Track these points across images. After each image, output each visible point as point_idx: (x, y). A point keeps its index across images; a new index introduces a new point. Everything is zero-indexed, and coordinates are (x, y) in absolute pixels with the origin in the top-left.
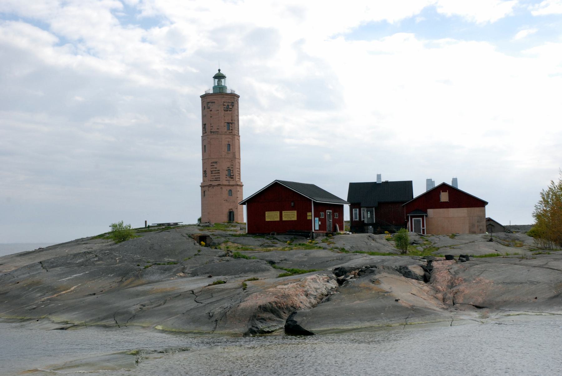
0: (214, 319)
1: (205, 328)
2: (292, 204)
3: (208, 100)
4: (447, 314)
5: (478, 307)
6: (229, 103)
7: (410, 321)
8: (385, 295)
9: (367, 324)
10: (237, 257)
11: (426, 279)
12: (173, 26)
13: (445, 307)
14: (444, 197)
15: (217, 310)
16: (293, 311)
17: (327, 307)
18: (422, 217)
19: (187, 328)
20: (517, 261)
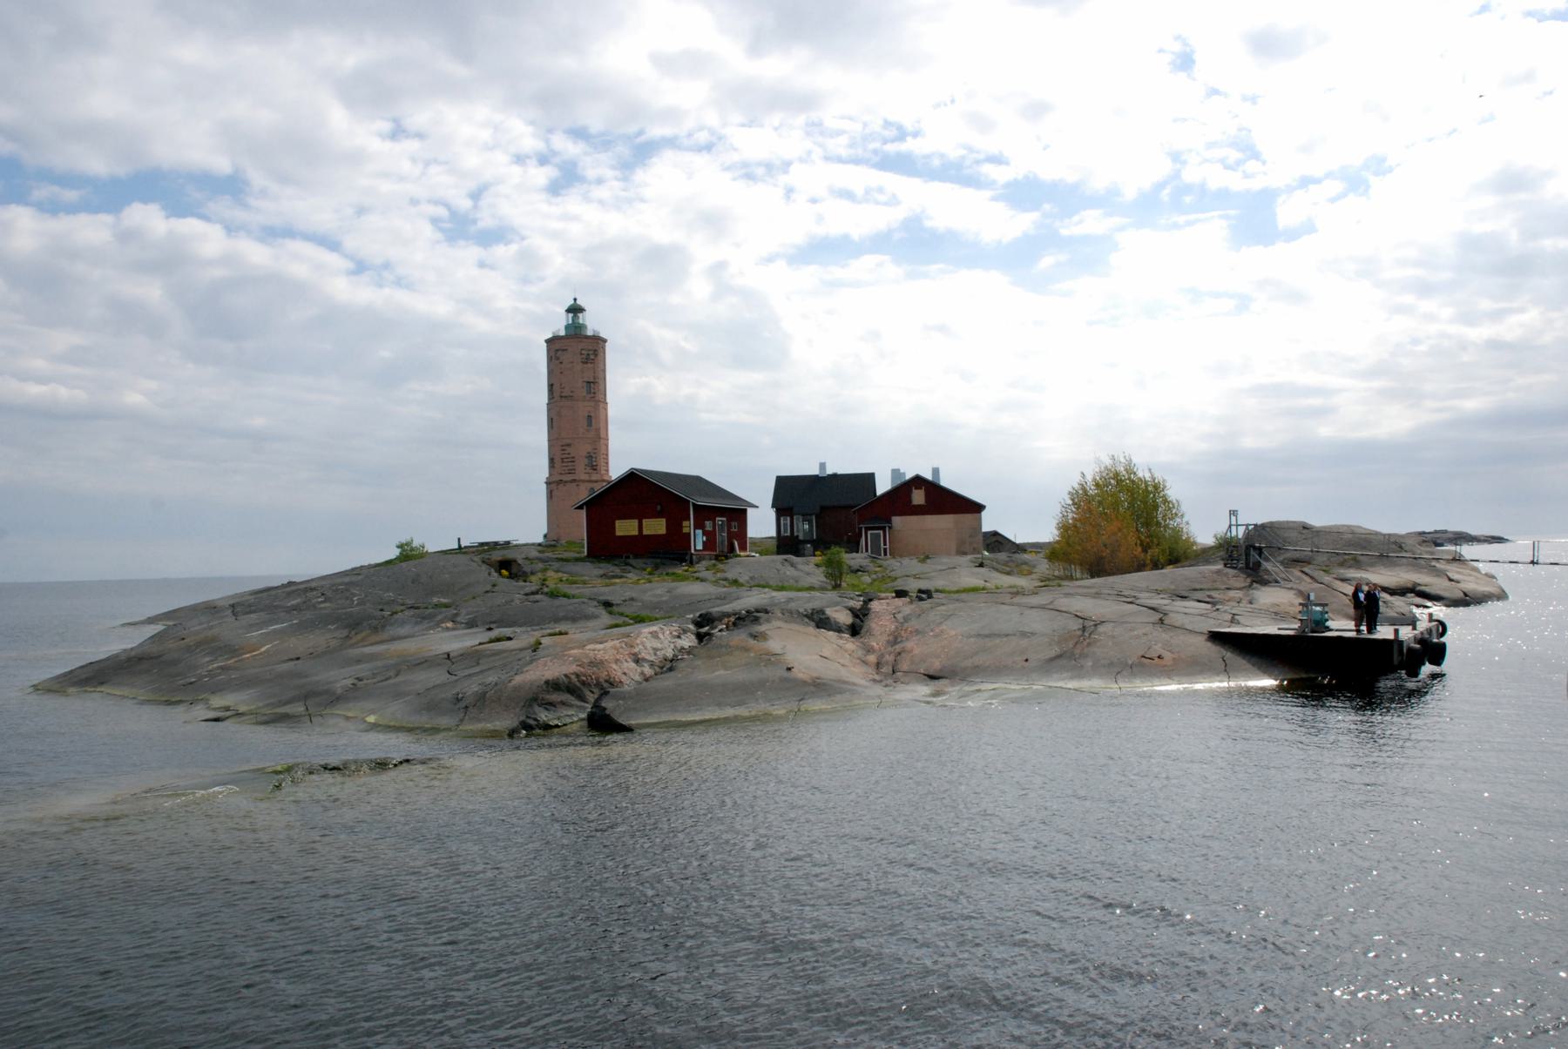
0: (462, 704)
1: (444, 721)
3: (557, 346)
4: (878, 690)
5: (932, 677)
7: (805, 706)
8: (770, 659)
9: (729, 712)
10: (553, 595)
11: (854, 631)
12: (525, 243)
13: (877, 677)
14: (918, 497)
15: (472, 688)
16: (606, 687)
17: (668, 681)
18: (883, 529)
19: (424, 720)
20: (1007, 599)
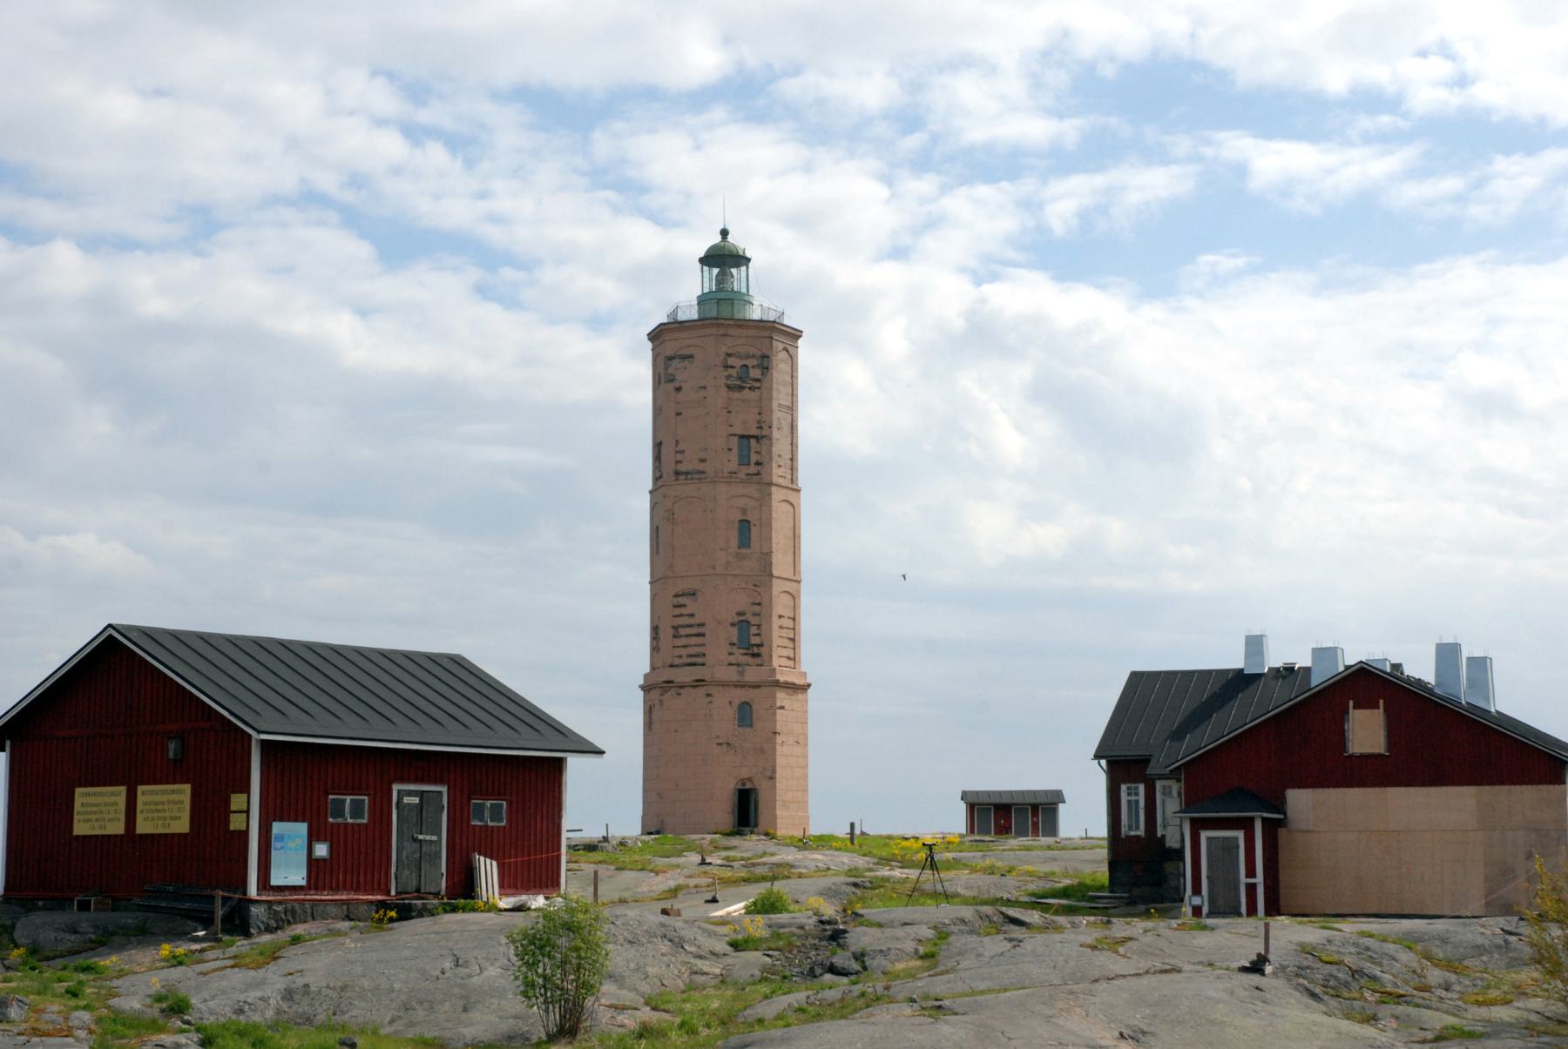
2: (172, 748)
6: (747, 357)
14: (1366, 731)
18: (1246, 825)
